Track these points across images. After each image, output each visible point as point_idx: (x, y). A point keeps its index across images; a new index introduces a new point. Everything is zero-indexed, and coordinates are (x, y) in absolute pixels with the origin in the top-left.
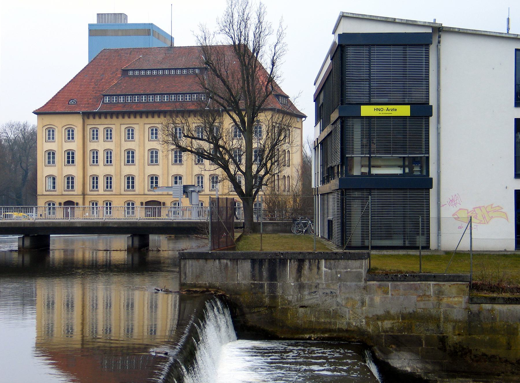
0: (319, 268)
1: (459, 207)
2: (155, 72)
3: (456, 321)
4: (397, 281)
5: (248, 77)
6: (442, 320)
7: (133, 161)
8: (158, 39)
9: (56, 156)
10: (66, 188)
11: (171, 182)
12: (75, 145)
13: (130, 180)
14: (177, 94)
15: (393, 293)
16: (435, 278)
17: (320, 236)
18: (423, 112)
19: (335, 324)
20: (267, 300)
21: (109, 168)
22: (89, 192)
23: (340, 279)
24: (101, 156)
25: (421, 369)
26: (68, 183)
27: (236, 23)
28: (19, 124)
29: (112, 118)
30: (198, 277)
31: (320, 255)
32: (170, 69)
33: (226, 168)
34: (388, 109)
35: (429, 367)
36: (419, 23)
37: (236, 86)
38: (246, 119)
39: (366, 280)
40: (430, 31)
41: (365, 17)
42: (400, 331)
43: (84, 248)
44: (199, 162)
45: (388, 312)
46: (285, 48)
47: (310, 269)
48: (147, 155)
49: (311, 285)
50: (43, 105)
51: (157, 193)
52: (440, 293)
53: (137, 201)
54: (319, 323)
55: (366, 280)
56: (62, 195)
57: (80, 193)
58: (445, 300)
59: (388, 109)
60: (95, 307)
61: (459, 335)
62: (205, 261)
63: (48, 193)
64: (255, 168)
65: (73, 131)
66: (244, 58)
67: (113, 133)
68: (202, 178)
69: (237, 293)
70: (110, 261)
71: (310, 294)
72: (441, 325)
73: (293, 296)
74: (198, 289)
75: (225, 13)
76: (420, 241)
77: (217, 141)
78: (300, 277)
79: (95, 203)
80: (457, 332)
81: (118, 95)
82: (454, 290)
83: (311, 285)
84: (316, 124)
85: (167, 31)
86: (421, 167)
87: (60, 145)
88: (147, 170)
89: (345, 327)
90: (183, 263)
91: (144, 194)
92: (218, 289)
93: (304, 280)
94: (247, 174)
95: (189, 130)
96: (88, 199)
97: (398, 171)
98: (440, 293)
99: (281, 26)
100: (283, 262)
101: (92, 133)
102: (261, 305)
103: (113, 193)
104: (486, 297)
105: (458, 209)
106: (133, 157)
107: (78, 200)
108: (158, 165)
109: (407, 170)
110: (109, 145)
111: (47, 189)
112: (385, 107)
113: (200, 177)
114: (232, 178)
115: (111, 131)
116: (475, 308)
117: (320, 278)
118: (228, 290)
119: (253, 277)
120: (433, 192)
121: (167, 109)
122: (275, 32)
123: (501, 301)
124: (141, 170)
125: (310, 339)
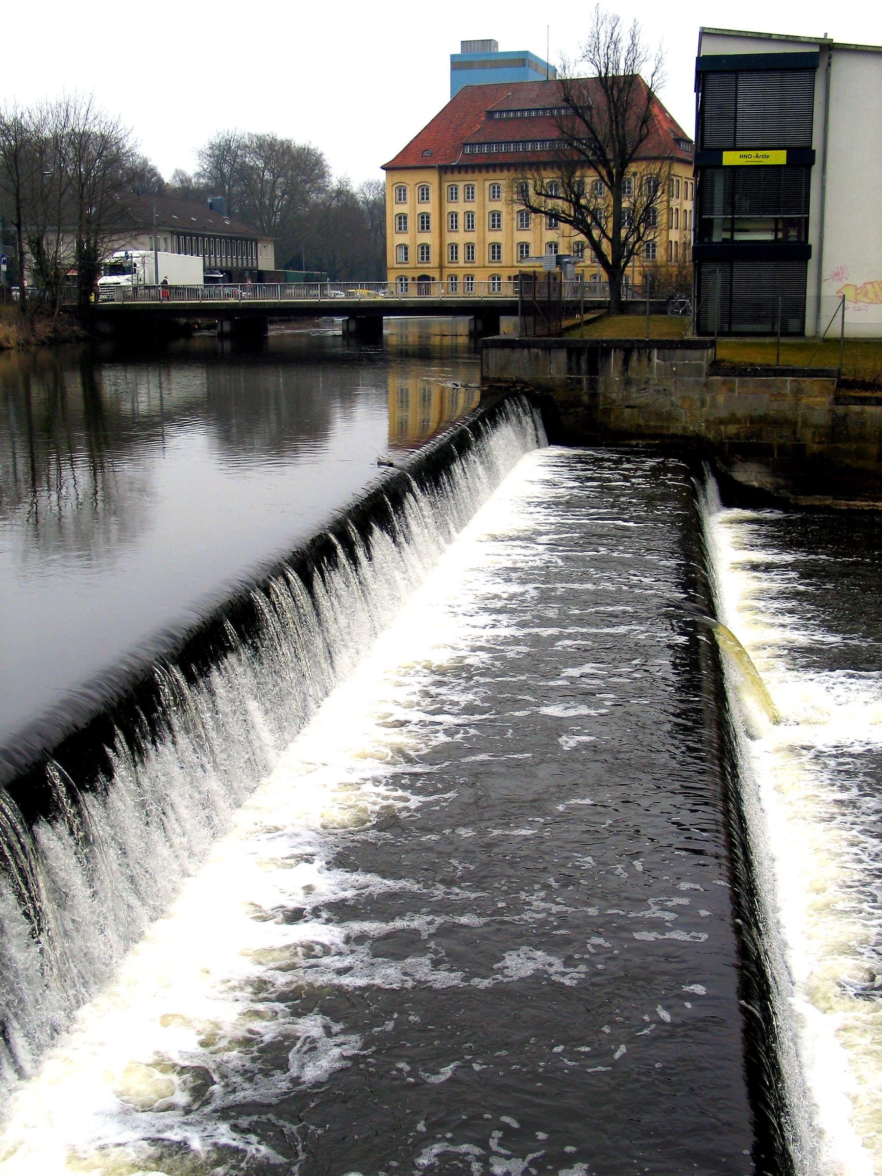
0: (650, 360)
1: (845, 282)
3: (816, 427)
4: (746, 376)
5: (616, 117)
6: (800, 424)
7: (499, 226)
9: (409, 219)
12: (431, 208)
13: (496, 248)
14: (499, 143)
15: (741, 391)
16: (793, 372)
18: (803, 158)
19: (668, 428)
20: (585, 398)
22: (446, 264)
23: (675, 373)
25: (771, 484)
29: (487, 172)
30: (503, 369)
31: (651, 343)
33: (588, 234)
34: (757, 156)
35: (781, 482)
36: (803, 40)
37: (603, 129)
38: (614, 171)
39: (708, 375)
40: (816, 49)
41: (732, 33)
42: (747, 437)
44: (551, 227)
45: (733, 415)
47: (639, 360)
52: (798, 392)
54: (649, 427)
55: (708, 375)
56: (416, 268)
57: (437, 265)
58: (804, 401)
59: (757, 156)
61: (820, 443)
62: (510, 350)
63: (399, 266)
64: (623, 233)
66: (612, 92)
71: (638, 391)
72: (799, 430)
73: (617, 393)
76: (793, 325)
77: (578, 197)
78: (626, 370)
80: (817, 440)
82: (816, 388)
85: (544, 58)
86: (799, 232)
87: (411, 208)
88: (496, 239)
89: (679, 432)
92: (526, 385)
93: (632, 375)
94: (616, 242)
95: (542, 186)
96: (447, 272)
97: (768, 237)
98: (798, 392)
99: (660, 50)
100: (607, 354)
101: (450, 191)
102: (578, 403)
103: (476, 265)
104: (854, 397)
105: (843, 284)
106: (499, 221)
107: (435, 274)
109: (780, 235)
110: (470, 207)
112: (760, 153)
114: (596, 246)
115: (473, 188)
116: (840, 410)
117: (651, 372)
119: (570, 370)
120: (812, 263)
122: (653, 58)
123: (873, 401)
125: (637, 446)
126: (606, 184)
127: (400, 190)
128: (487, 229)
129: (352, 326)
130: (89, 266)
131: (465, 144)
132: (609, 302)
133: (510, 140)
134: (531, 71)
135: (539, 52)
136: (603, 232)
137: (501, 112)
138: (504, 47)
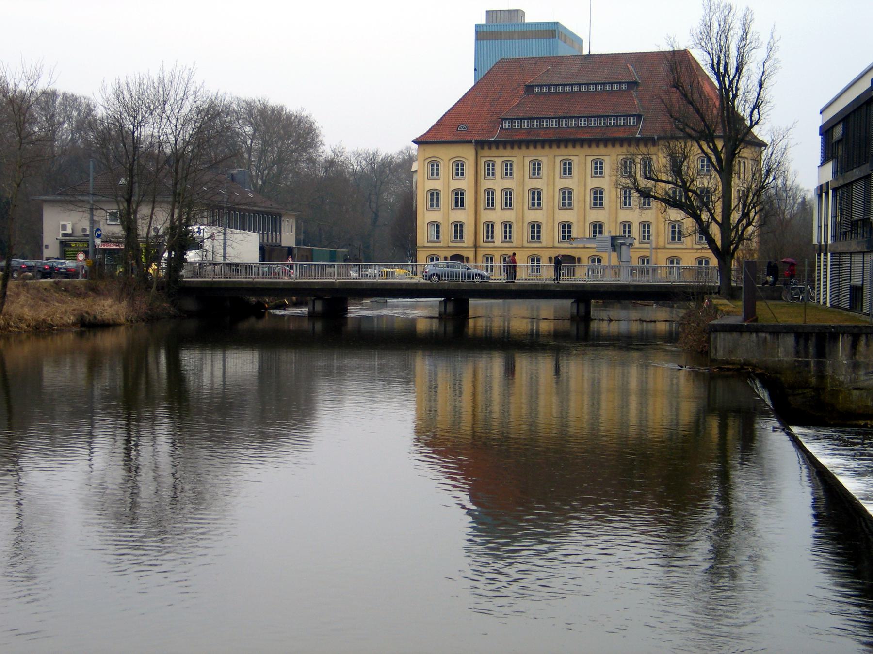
2: (568, 89)
7: (539, 204)
8: (565, 42)
9: (441, 197)
10: (453, 238)
11: (588, 233)
12: (465, 184)
13: (536, 229)
17: (828, 305)
20: (813, 381)
21: (508, 212)
22: (481, 243)
24: (499, 198)
26: (456, 232)
27: (715, 36)
28: (367, 153)
29: (512, 148)
30: (731, 352)
32: (588, 84)
33: (698, 218)
43: (517, 317)
46: (778, 65)
48: (558, 197)
49: (868, 364)
50: (425, 132)
51: (574, 245)
53: (545, 255)
56: (449, 247)
57: (471, 244)
60: (488, 389)
62: (739, 334)
65: (462, 165)
67: (514, 168)
68: (629, 227)
69: (776, 372)
70: (508, 331)
71: (866, 374)
74: (731, 367)
75: (701, 22)
78: (854, 354)
79: (489, 258)
81: (521, 119)
83: (868, 364)
84: (824, 162)
90: (713, 336)
91: (554, 247)
92: (754, 367)
94: (725, 226)
96: (481, 252)
99: (772, 37)
100: (834, 337)
101: (486, 168)
106: (539, 199)
107: (470, 254)
108: (572, 209)
110: (508, 184)
111: (429, 239)
113: (627, 225)
114: (704, 230)
115: (511, 165)
118: (767, 368)
119: (797, 354)
121: (586, 136)
122: (765, 45)
124: (550, 217)
125: (865, 426)
126: (716, 170)
127: (433, 166)
128: (526, 207)
129: (450, 308)
130: (182, 241)
131: (503, 119)
132: (719, 287)
133: (552, 115)
134: (560, 43)
135: (573, 24)
136: (712, 215)
137: (541, 86)
138: (531, 18)
